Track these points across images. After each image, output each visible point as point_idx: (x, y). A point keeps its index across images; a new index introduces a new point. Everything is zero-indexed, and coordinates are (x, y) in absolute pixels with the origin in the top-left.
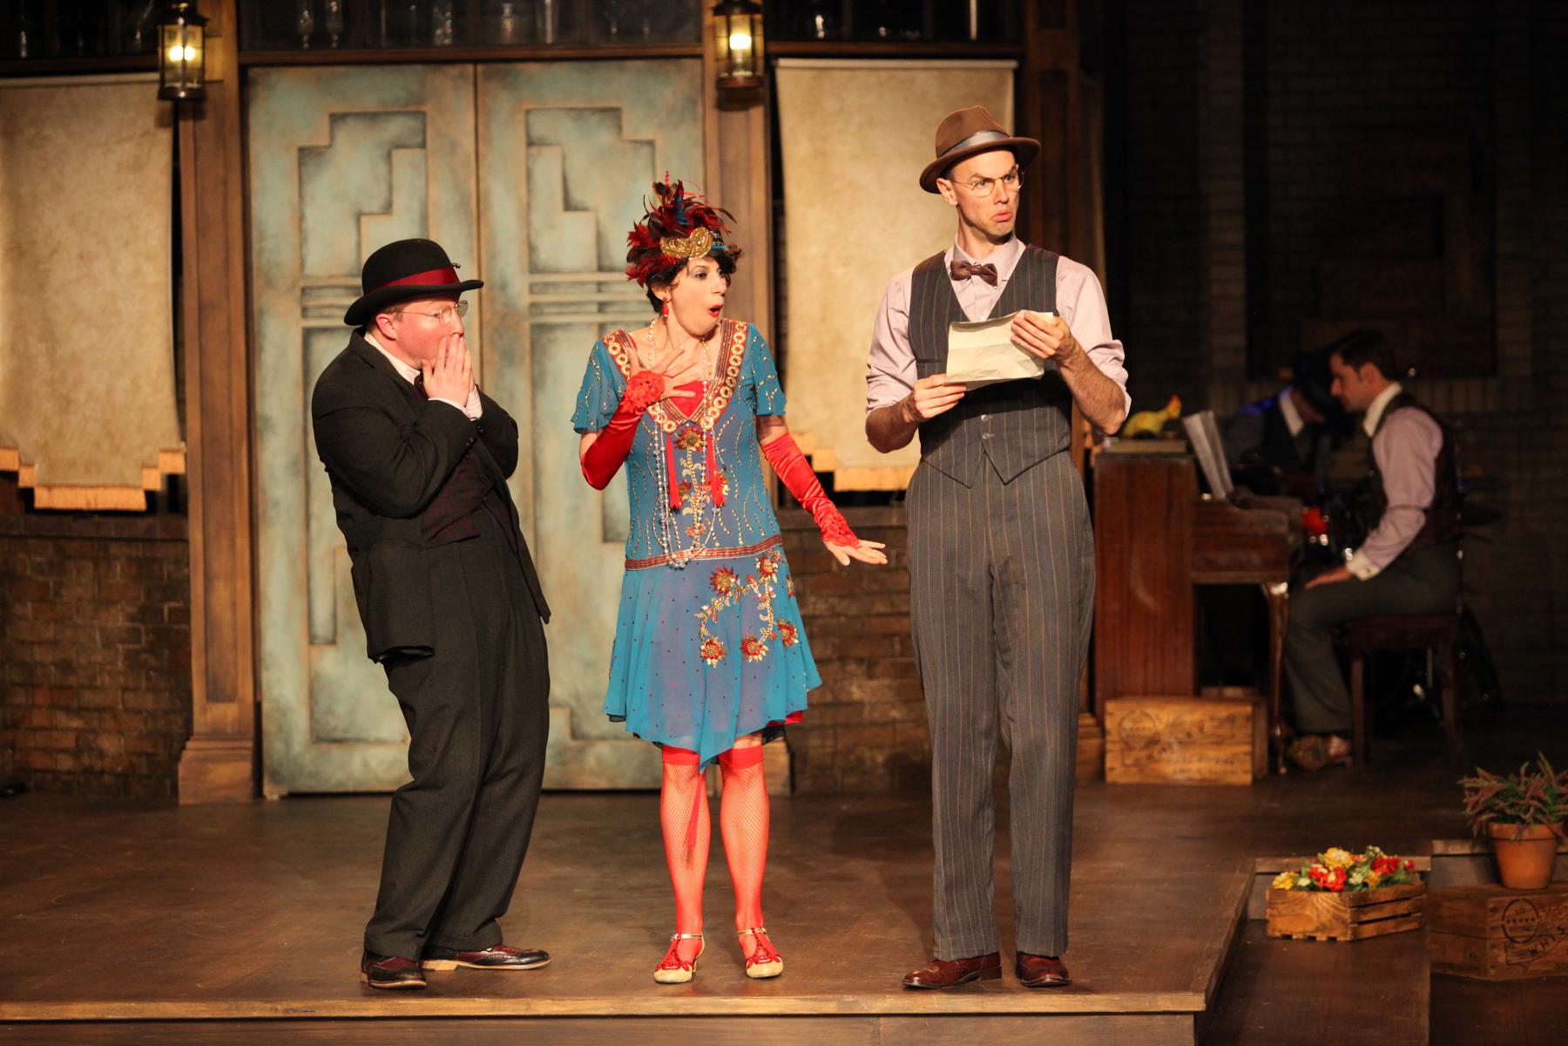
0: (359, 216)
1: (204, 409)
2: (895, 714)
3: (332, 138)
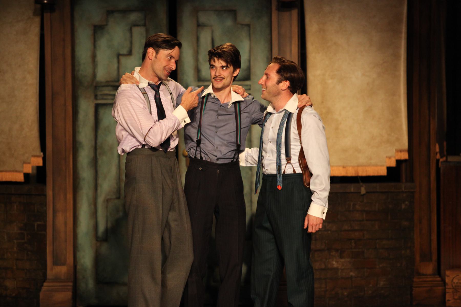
0: (119, 56)
1: (54, 138)
2: (352, 274)
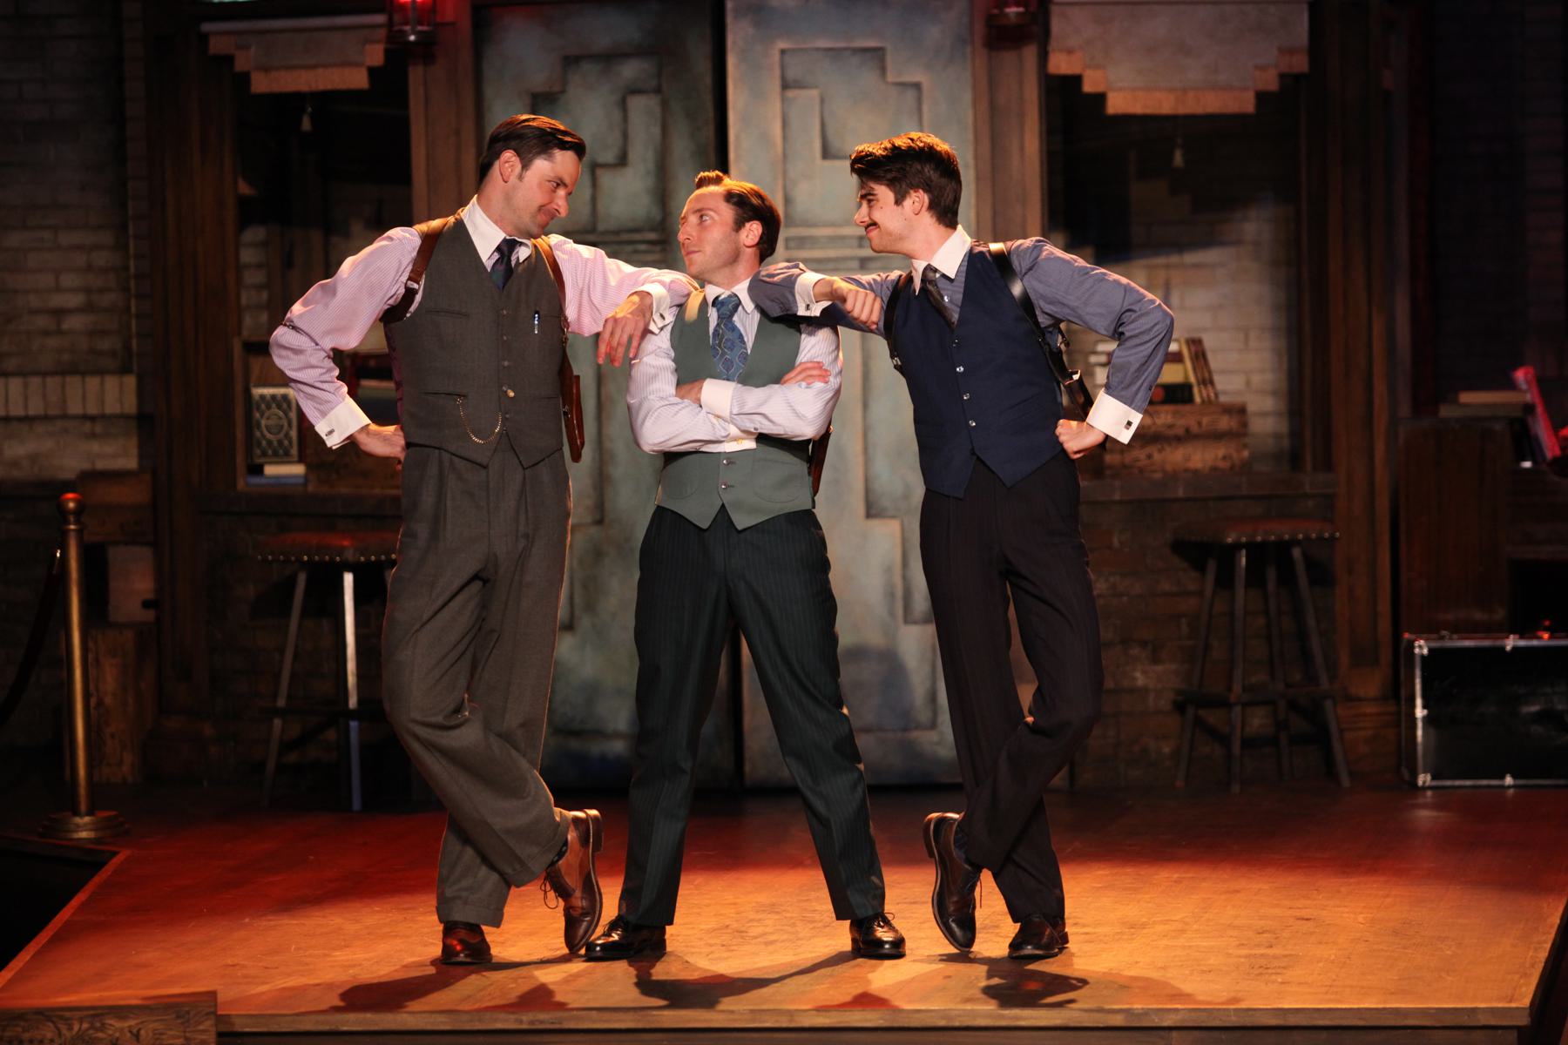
3: (564, 82)
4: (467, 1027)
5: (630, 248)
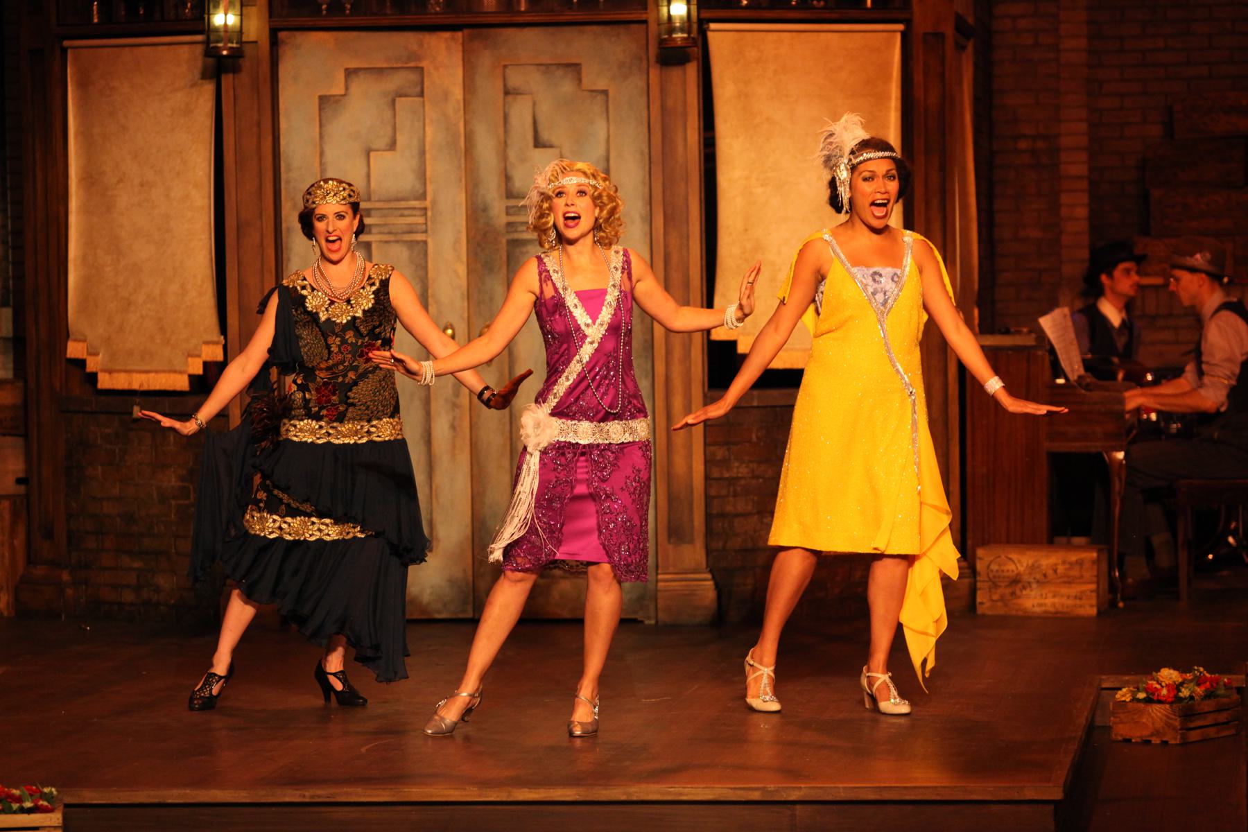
4: (263, 800)
5: (399, 212)
